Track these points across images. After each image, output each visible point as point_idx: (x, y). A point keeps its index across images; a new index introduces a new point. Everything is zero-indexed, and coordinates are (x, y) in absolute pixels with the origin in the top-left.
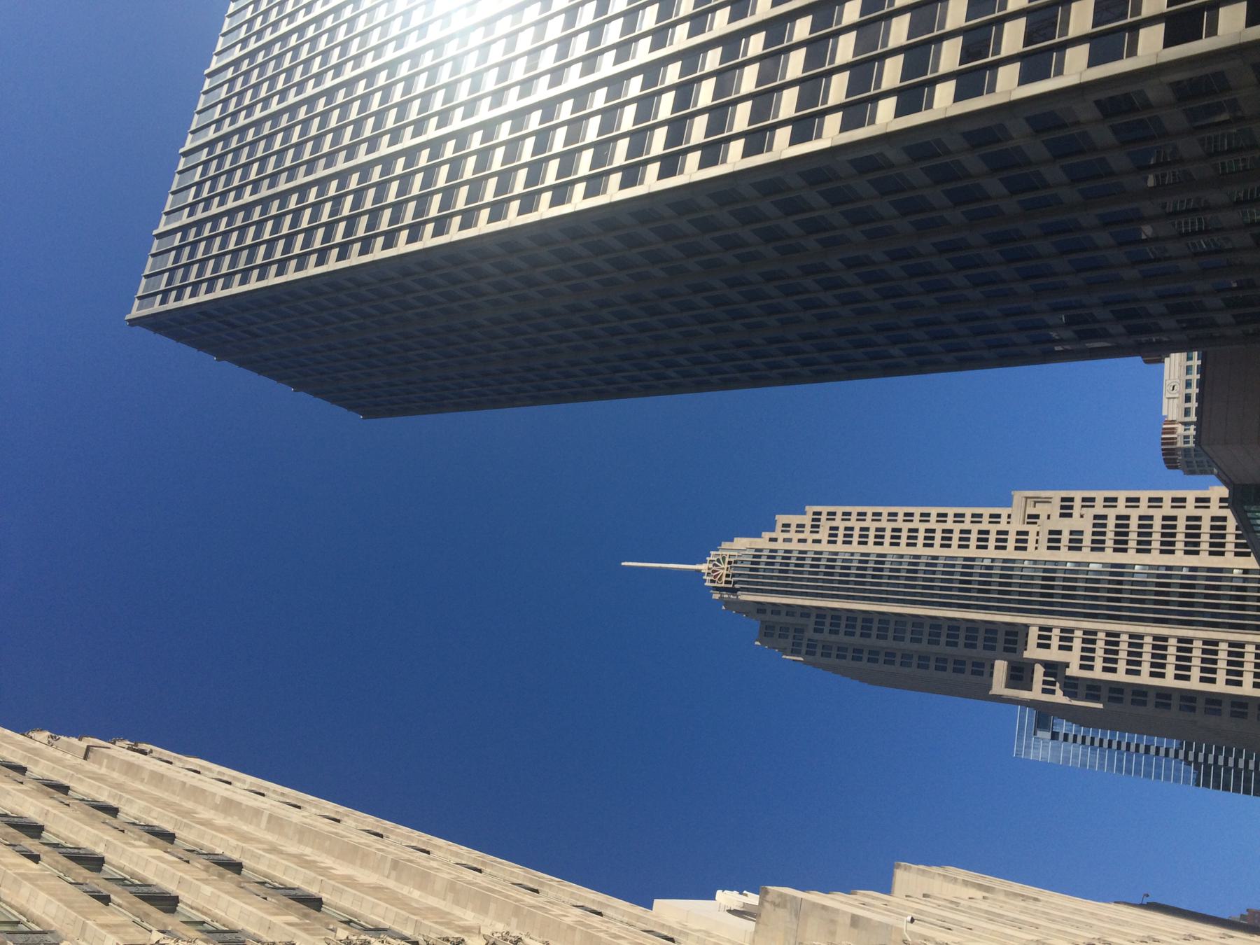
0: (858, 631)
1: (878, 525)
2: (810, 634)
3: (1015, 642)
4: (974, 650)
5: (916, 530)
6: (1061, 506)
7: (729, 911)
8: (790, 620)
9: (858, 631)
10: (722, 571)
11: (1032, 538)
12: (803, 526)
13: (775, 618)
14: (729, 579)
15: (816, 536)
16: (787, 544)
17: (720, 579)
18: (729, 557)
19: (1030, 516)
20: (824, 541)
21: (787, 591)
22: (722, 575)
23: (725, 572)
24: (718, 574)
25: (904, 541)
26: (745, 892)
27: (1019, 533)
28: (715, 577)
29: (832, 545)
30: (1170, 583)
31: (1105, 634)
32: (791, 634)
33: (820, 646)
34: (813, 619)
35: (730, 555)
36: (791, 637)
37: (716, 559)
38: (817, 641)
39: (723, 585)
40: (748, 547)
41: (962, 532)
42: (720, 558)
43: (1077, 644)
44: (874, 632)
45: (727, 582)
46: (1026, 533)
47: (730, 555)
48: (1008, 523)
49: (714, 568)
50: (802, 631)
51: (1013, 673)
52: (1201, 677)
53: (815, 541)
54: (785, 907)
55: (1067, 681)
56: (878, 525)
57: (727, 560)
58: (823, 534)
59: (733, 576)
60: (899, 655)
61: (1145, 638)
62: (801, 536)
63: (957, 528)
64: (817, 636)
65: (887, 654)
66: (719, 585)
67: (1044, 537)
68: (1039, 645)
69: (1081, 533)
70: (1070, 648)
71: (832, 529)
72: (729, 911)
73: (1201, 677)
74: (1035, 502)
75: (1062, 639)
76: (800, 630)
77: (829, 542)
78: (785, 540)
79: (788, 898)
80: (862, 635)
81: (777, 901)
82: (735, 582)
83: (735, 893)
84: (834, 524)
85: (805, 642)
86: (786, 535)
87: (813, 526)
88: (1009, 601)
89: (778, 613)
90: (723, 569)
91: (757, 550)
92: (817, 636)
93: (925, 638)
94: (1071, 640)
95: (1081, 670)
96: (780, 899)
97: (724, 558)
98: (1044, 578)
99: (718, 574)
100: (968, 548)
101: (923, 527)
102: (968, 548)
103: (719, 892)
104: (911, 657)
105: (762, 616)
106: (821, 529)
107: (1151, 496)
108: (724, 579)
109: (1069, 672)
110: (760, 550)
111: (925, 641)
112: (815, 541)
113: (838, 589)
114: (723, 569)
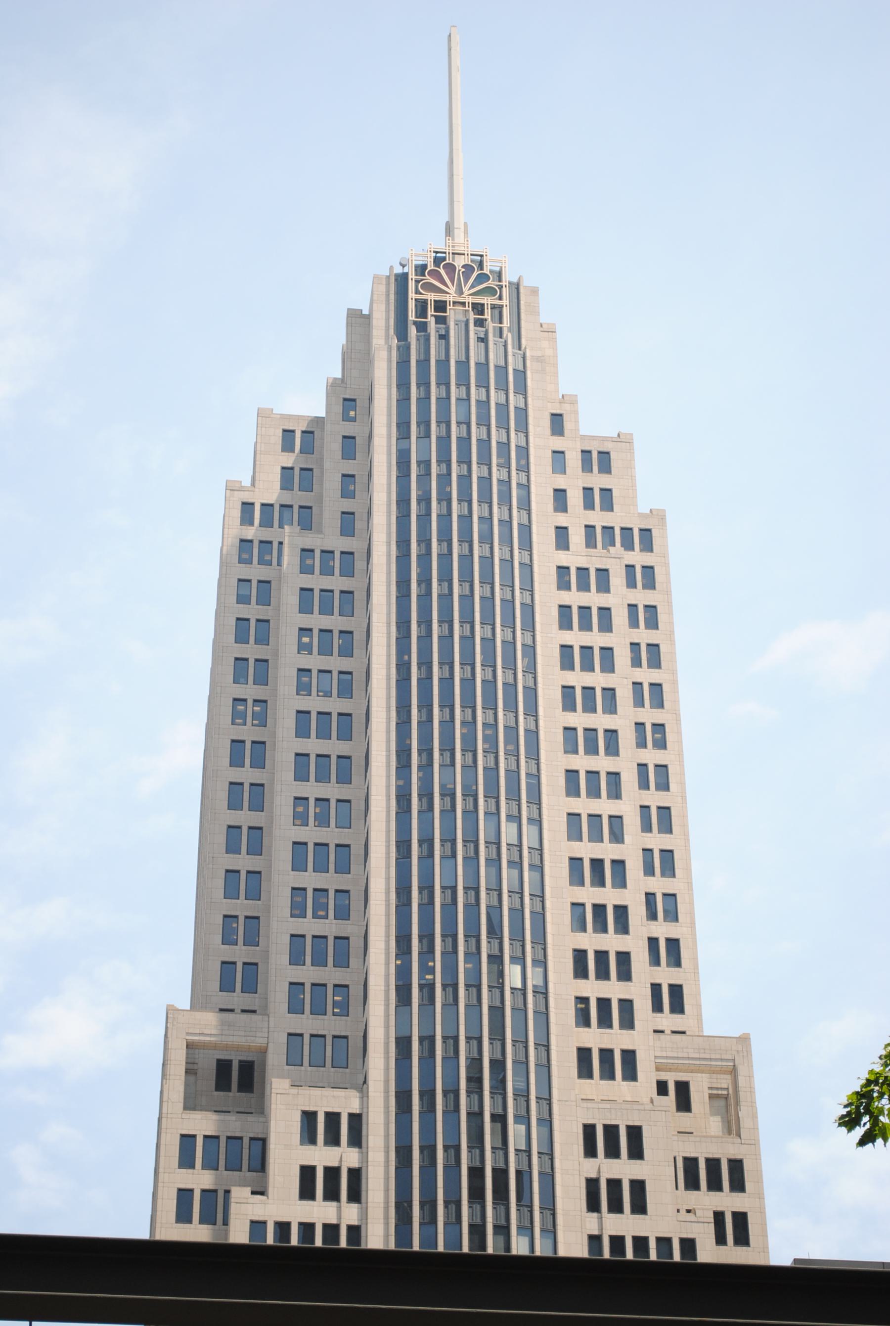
3: (318, 1062)
5: (625, 975)
6: (718, 1161)
8: (331, 483)
10: (452, 290)
14: (431, 311)
16: (547, 422)
18: (493, 307)
19: (683, 1089)
21: (408, 542)
23: (451, 296)
24: (447, 287)
27: (629, 1057)
28: (435, 274)
30: (506, 1198)
31: (356, 1223)
32: (297, 498)
34: (338, 543)
35: (501, 307)
36: (287, 499)
37: (486, 271)
39: (412, 295)
40: (528, 354)
42: (491, 283)
44: (313, 746)
46: (631, 1074)
47: (501, 307)
52: (264, 1223)
55: (221, 1194)
57: (487, 301)
61: (354, 1207)
64: (290, 559)
66: (411, 285)
68: (309, 1117)
69: (640, 1207)
70: (307, 1192)
73: (264, 1223)
74: (726, 1098)
75: (332, 1173)
77: (563, 570)
78: (558, 454)
80: (303, 714)
86: (575, 498)
88: (426, 705)
89: (347, 493)
90: (460, 292)
91: (521, 375)
92: (290, 559)
95: (248, 1223)
97: (490, 291)
98: (500, 1175)
99: (447, 287)
100: (581, 1075)
102: (581, 1075)
108: (431, 297)
109: (240, 1194)
110: (522, 389)
113: (425, 596)
114: (460, 292)
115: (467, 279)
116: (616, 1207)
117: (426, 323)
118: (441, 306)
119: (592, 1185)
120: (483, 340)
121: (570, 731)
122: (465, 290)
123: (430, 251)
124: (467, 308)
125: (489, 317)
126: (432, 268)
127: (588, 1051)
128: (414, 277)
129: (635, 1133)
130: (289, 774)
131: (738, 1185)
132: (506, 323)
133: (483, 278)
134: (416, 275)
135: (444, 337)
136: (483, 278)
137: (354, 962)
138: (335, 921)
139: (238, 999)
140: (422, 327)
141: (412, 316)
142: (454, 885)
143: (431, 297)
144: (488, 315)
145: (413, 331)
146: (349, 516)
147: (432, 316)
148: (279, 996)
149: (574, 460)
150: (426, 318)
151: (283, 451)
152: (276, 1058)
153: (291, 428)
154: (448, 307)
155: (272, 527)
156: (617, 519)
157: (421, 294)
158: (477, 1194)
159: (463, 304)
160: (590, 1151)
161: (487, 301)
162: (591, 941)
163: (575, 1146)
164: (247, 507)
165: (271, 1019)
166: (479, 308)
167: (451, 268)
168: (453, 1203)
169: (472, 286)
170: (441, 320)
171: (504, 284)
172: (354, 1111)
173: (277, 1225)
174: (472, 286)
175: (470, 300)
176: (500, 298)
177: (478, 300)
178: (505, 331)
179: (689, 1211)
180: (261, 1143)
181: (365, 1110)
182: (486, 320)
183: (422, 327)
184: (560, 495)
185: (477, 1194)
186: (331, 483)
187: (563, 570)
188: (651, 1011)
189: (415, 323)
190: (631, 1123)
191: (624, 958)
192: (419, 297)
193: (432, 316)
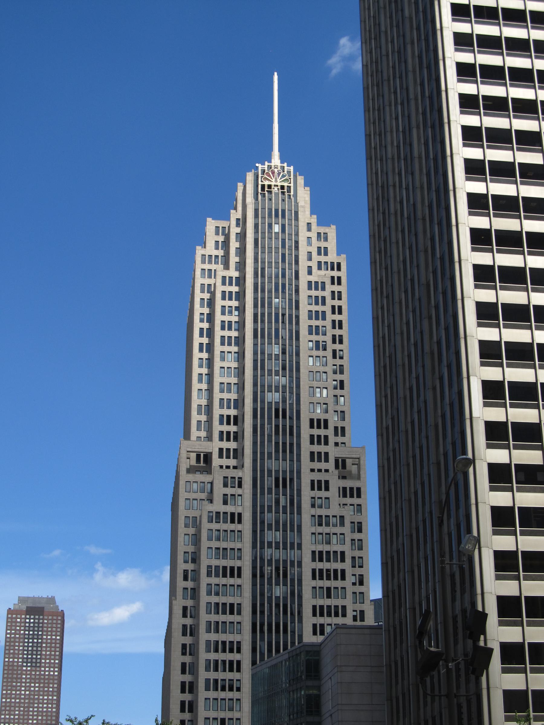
10: (274, 180)
11: (323, 465)
12: (326, 254)
14: (266, 189)
18: (288, 186)
19: (344, 461)
23: (273, 184)
24: (272, 179)
27: (326, 454)
28: (268, 174)
39: (260, 183)
43: (229, 509)
67: (322, 477)
71: (323, 283)
85: (213, 267)
87: (326, 263)
90: (276, 181)
99: (272, 179)
114: (276, 181)
115: (278, 177)
116: (320, 489)
117: (265, 193)
119: (314, 571)
120: (283, 200)
121: (311, 327)
122: (278, 180)
124: (279, 187)
125: (286, 191)
126: (267, 172)
127: (313, 436)
128: (261, 175)
131: (359, 496)
132: (292, 193)
134: (261, 175)
135: (270, 200)
138: (234, 362)
140: (264, 195)
144: (286, 190)
147: (267, 191)
148: (216, 436)
150: (265, 191)
151: (215, 235)
152: (215, 456)
153: (218, 226)
154: (272, 187)
155: (212, 577)
157: (263, 182)
158: (277, 416)
159: (277, 186)
160: (313, 489)
161: (286, 184)
162: (314, 308)
163: (308, 487)
165: (214, 443)
167: (273, 173)
168: (270, 418)
169: (281, 179)
170: (270, 192)
171: (291, 177)
172: (240, 476)
173: (215, 604)
174: (281, 179)
175: (279, 184)
176: (290, 183)
177: (283, 184)
178: (292, 197)
181: (243, 476)
182: (285, 192)
183: (264, 195)
185: (277, 416)
187: (310, 283)
188: (334, 436)
190: (325, 479)
191: (324, 298)
192: (262, 183)
193: (267, 191)
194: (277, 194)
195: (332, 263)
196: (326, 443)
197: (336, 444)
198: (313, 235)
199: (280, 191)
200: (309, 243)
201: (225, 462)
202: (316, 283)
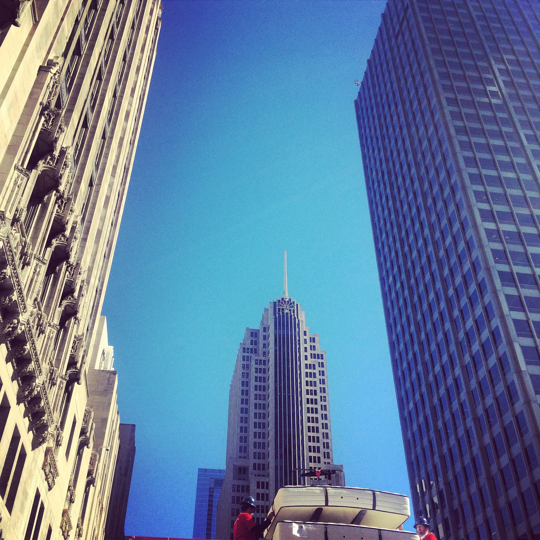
0: (258, 384)
1: (318, 391)
2: (254, 357)
4: (253, 447)
7: (67, 460)
8: (261, 346)
9: (258, 384)
12: (314, 349)
13: (261, 338)
15: (309, 357)
17: (281, 306)
20: (306, 362)
22: (282, 306)
24: (283, 304)
25: (310, 415)
26: (114, 359)
29: (306, 393)
33: (248, 363)
34: (263, 358)
37: (292, 302)
38: (251, 361)
39: (277, 307)
41: (318, 447)
45: (279, 309)
48: (325, 463)
49: (286, 303)
50: (256, 353)
51: (242, 469)
53: (306, 356)
54: (108, 384)
56: (318, 391)
57: (292, 309)
58: (310, 361)
59: (283, 313)
60: (248, 371)
62: (309, 349)
63: (319, 425)
65: (247, 400)
71: (314, 365)
72: (67, 460)
76: (256, 351)
77: (306, 365)
79: (112, 391)
81: (111, 380)
82: (279, 314)
83: (113, 355)
84: (317, 366)
86: (309, 349)
87: (315, 354)
88: (281, 437)
90: (286, 307)
93: (257, 420)
94: (263, 500)
96: (112, 381)
97: (293, 307)
101: (319, 416)
103: (112, 347)
104: (246, 413)
105: (261, 330)
106: (313, 359)
107: (325, 380)
108: (281, 308)
111: (256, 392)
112: (306, 356)
114: (286, 307)
118: (283, 309)
122: (288, 306)
123: (258, 181)
129: (322, 355)
130: (254, 380)
133: (291, 304)
136: (291, 304)
137: (266, 448)
139: (243, 454)
141: (277, 312)
142: (329, 505)
143: (281, 308)
145: (277, 315)
146: (264, 353)
148: (251, 455)
149: (308, 341)
152: (251, 468)
156: (316, 352)
164: (244, 349)
166: (290, 311)
167: (285, 302)
179: (66, 188)
180: (248, 487)
184: (306, 348)
186: (261, 346)
187: (306, 365)
189: (278, 313)
194: (287, 313)
195: (318, 355)
196: (319, 462)
197: (325, 463)
198: (308, 346)
199: (289, 312)
200: (306, 343)
201: (257, 472)
202: (310, 365)
